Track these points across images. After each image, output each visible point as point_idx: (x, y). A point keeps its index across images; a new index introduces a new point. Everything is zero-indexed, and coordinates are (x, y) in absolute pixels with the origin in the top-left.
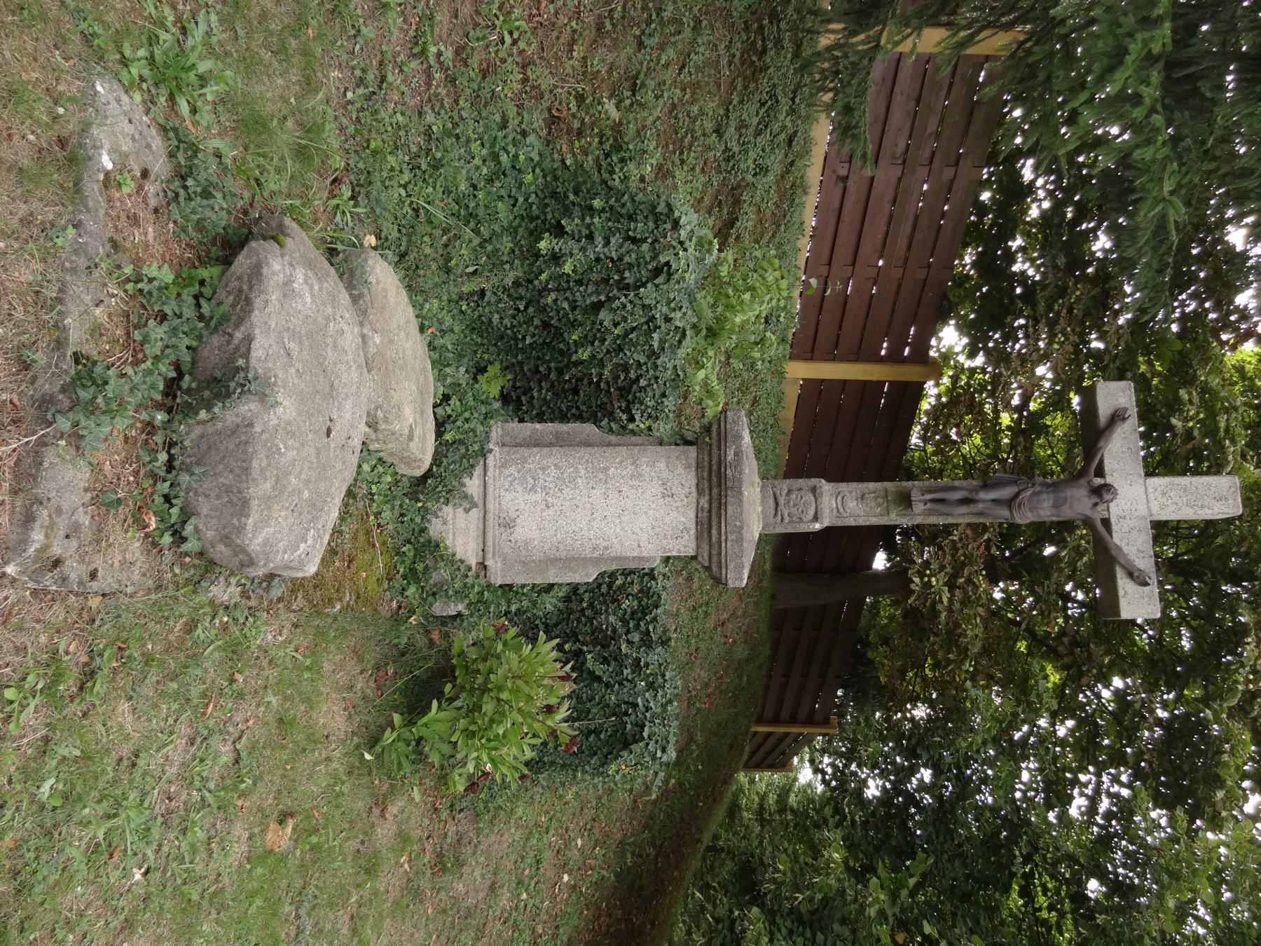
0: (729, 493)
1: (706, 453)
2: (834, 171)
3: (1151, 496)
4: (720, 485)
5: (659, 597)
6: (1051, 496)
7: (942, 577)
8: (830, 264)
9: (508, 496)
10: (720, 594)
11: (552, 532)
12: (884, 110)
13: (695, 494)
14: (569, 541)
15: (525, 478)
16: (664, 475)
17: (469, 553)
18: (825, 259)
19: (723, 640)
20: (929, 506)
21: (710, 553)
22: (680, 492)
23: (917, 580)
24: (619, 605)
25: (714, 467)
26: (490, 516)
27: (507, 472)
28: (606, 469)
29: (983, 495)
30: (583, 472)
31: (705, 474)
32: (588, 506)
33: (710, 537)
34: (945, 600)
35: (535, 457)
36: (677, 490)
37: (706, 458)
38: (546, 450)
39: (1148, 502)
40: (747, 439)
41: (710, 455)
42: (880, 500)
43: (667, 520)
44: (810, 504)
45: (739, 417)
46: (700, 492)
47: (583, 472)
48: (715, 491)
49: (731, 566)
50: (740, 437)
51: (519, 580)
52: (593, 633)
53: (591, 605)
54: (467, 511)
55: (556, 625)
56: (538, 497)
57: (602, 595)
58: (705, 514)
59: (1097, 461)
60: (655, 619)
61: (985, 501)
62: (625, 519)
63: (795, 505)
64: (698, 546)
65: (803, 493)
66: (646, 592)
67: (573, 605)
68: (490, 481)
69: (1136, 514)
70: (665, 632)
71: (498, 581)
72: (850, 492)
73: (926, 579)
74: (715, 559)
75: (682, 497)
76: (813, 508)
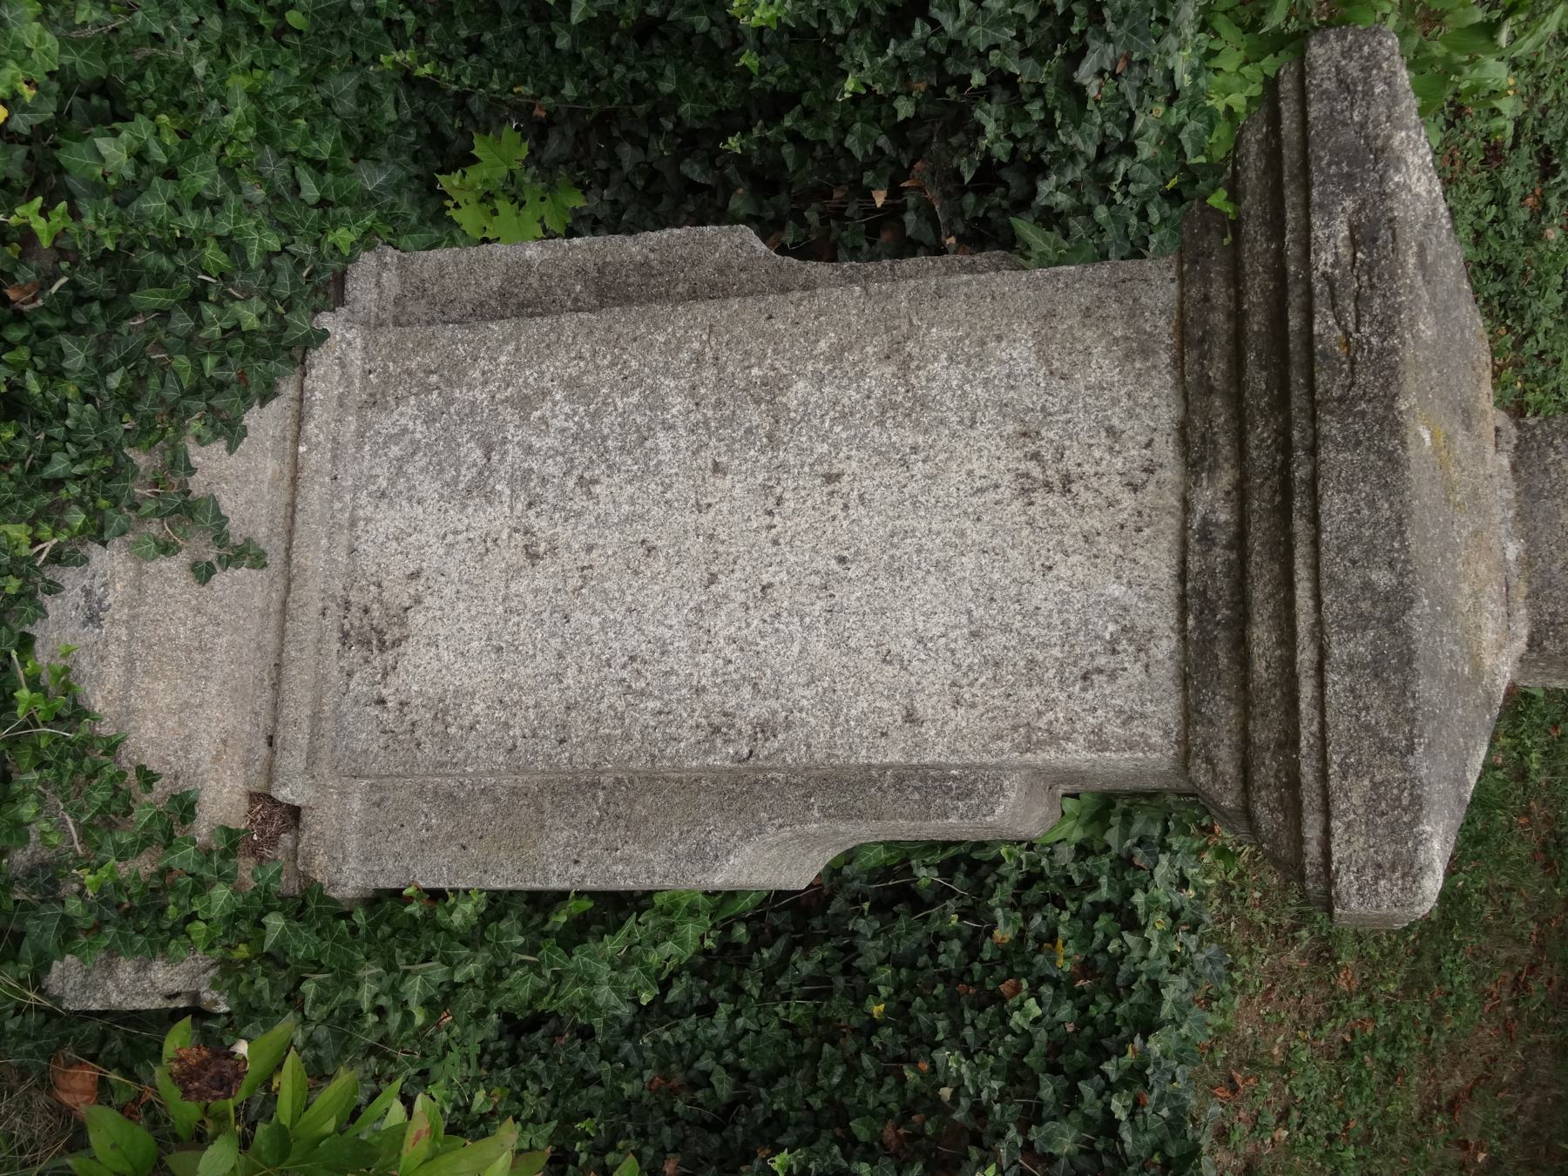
0: (1330, 426)
1: (1217, 272)
4: (1282, 401)
5: (1155, 988)
9: (387, 521)
10: (1438, 1012)
11: (546, 662)
13: (1171, 473)
14: (612, 697)
15: (452, 444)
16: (1028, 396)
17: (204, 750)
21: (1245, 744)
22: (1102, 467)
24: (1004, 1018)
26: (310, 594)
27: (385, 424)
28: (774, 386)
30: (678, 404)
31: (1217, 370)
32: (695, 545)
33: (1243, 661)
35: (498, 357)
36: (1088, 456)
37: (1220, 293)
38: (536, 328)
40: (1416, 179)
41: (1236, 278)
43: (1041, 594)
45: (1371, 64)
46: (1195, 460)
47: (678, 404)
48: (1261, 433)
49: (1352, 797)
50: (1373, 156)
51: (431, 872)
52: (907, 1112)
53: (901, 1013)
54: (203, 573)
55: (770, 1079)
56: (496, 517)
57: (946, 977)
58: (1220, 556)
60: (1136, 1076)
62: (850, 596)
64: (1190, 714)
66: (1102, 972)
67: (837, 1008)
68: (315, 459)
70: (1175, 1125)
71: (349, 878)
74: (1268, 768)
75: (1114, 487)
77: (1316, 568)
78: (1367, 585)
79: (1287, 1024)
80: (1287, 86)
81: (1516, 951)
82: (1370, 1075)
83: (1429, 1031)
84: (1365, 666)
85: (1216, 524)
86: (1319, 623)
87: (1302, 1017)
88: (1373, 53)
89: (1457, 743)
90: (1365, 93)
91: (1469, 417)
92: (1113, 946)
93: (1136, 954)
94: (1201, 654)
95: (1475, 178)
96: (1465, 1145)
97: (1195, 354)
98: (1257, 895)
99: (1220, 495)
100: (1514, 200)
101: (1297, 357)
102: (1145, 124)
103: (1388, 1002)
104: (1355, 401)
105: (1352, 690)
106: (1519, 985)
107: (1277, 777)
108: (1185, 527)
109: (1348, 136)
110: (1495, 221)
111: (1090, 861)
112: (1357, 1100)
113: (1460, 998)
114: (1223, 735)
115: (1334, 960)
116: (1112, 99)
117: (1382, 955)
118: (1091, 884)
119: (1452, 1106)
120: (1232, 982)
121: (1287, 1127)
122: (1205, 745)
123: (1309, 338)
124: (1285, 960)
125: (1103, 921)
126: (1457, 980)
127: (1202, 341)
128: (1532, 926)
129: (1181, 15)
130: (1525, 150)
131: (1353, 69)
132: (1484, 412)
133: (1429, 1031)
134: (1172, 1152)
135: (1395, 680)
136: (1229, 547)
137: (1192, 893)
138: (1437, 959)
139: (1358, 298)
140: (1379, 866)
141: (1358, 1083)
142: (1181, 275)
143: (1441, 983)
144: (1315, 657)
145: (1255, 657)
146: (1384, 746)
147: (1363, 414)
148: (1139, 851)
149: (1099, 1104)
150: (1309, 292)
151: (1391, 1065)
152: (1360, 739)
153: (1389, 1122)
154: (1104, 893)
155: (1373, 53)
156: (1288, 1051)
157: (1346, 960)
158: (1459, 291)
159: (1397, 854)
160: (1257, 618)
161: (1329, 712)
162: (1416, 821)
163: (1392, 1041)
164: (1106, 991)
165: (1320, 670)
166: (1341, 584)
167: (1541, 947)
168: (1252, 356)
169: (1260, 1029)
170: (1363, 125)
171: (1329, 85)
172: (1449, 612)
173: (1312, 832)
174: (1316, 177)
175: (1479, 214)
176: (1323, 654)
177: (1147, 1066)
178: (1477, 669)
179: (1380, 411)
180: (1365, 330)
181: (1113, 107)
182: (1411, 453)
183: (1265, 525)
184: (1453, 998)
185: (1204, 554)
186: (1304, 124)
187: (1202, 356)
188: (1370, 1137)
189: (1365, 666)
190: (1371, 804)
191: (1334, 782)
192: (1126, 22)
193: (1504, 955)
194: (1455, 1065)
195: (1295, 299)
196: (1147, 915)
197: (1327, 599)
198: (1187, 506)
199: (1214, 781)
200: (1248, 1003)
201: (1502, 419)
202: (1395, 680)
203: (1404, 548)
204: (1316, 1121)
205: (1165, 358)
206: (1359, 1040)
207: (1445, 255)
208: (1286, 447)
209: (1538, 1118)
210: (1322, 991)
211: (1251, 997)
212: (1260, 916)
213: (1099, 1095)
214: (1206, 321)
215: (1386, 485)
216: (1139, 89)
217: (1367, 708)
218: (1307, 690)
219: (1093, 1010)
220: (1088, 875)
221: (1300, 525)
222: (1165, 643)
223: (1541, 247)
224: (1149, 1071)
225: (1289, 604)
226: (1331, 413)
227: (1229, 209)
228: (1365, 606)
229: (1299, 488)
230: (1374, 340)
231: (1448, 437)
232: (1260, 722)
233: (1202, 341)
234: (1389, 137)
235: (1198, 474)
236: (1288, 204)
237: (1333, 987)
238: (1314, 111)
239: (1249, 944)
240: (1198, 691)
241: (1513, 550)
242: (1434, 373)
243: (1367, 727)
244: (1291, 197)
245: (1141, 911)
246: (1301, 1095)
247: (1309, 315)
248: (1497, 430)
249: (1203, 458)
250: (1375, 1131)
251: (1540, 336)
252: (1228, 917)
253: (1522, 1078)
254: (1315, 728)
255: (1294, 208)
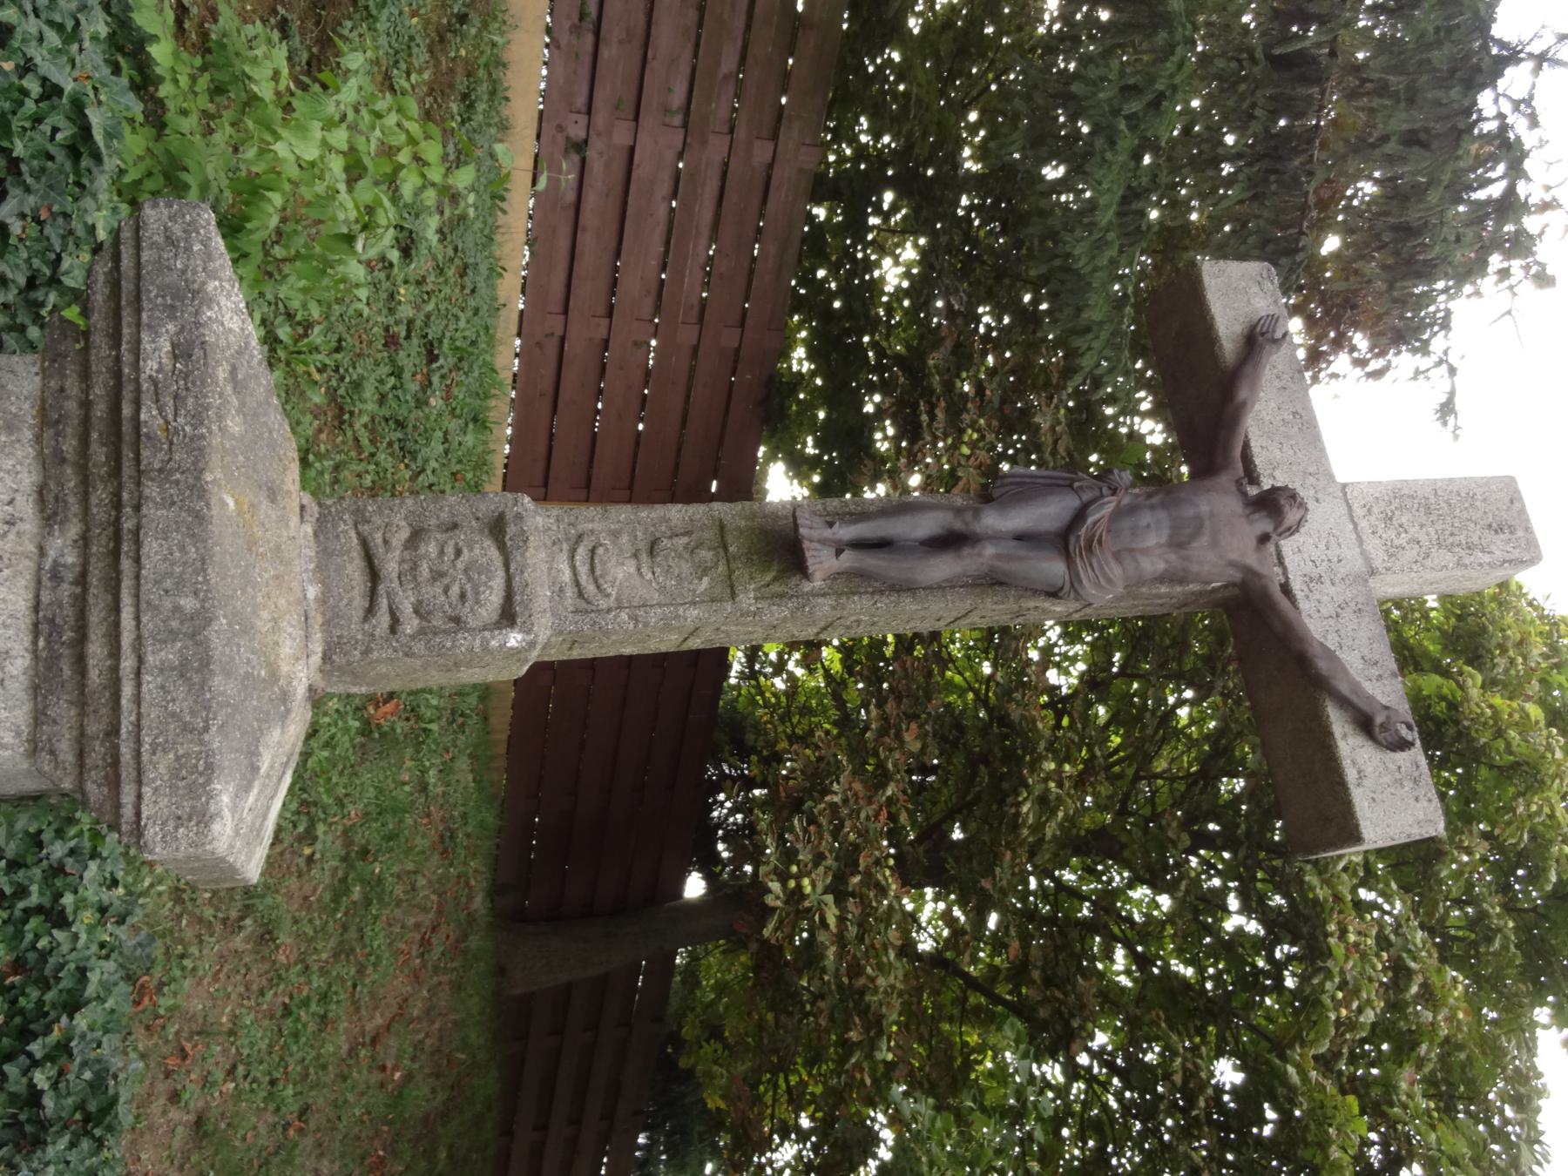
0: (151, 490)
1: (71, 370)
2: (560, 128)
3: (1363, 524)
4: (116, 471)
5: (82, 972)
6: (1162, 515)
7: (822, 876)
8: (566, 312)
10: (361, 971)
12: (641, 20)
18: (555, 303)
19: (376, 1077)
20: (848, 559)
23: (775, 886)
25: (100, 410)
29: (993, 521)
31: (69, 446)
33: (80, 662)
34: (832, 921)
37: (73, 386)
39: (1360, 541)
41: (85, 375)
42: (706, 555)
44: (487, 571)
46: (49, 510)
48: (100, 494)
49: (159, 768)
50: (187, 297)
58: (66, 591)
59: (1238, 452)
61: (996, 537)
63: (437, 575)
64: (39, 717)
65: (461, 537)
69: (1342, 571)
70: (98, 1085)
72: (615, 534)
73: (792, 884)
76: (498, 582)
77: (137, 596)
78: (177, 609)
79: (233, 997)
80: (126, 234)
81: (422, 918)
82: (305, 1026)
83: (355, 986)
84: (174, 669)
85: (64, 566)
86: (139, 638)
87: (247, 989)
88: (193, 221)
89: (250, 725)
90: (186, 249)
91: (274, 493)
92: (43, 943)
93: (65, 948)
94: (49, 669)
95: (379, 356)
96: (383, 1068)
97: (52, 432)
98: (207, 895)
99: (69, 542)
100: (407, 375)
101: (128, 437)
102: (71, 266)
103: (321, 968)
104: (171, 472)
105: (163, 687)
106: (425, 943)
107: (104, 759)
108: (40, 569)
109: (172, 278)
110: (394, 388)
111: (21, 873)
112: (295, 1048)
113: (379, 958)
114: (65, 731)
115: (274, 940)
116: (37, 240)
117: (315, 931)
118: (22, 892)
119: (374, 1041)
120: (183, 968)
121: (234, 1080)
122: (50, 740)
123: (137, 423)
124: (231, 945)
125: (34, 923)
126: (375, 944)
127: (58, 422)
128: (434, 897)
129: (96, 184)
130: (415, 341)
131: (177, 230)
132: (289, 492)
133: (355, 986)
134: (92, 1107)
135: (196, 678)
136: (75, 583)
137: (121, 891)
138: (360, 930)
139: (176, 397)
140: (179, 818)
141: (296, 1035)
142: (43, 370)
143: (364, 947)
144: (135, 665)
145: (90, 667)
146: (186, 728)
147: (177, 482)
148: (70, 860)
149: (24, 1080)
150: (138, 390)
151: (324, 1017)
152: (167, 724)
153: (322, 1061)
154: (34, 899)
155: (193, 221)
156: (235, 1018)
157: (283, 938)
158: (269, 404)
159: (193, 807)
160: (93, 637)
161: (144, 705)
162: (209, 781)
163: (324, 998)
164: (36, 983)
165: (138, 673)
166: (156, 608)
167: (440, 912)
168: (95, 435)
169: (209, 1004)
170: (184, 272)
171: (159, 239)
172: (247, 629)
173: (127, 798)
174: (145, 304)
175: (381, 382)
176: (141, 660)
177: (71, 1040)
178: (274, 675)
179: (191, 481)
180: (181, 420)
181: (38, 247)
182: (214, 512)
183: (101, 565)
184: (373, 958)
185: (54, 588)
186: (138, 265)
187: (57, 434)
188: (307, 1075)
189: (174, 669)
190: (175, 773)
191: (145, 757)
192: (43, 179)
193: (411, 921)
194: (376, 1008)
195: (127, 394)
196: (75, 912)
197: (144, 619)
198: (42, 552)
199: (56, 768)
200: (199, 984)
201: (307, 499)
202: (196, 678)
203: (206, 581)
204: (258, 1072)
205: (28, 435)
206: (296, 1001)
207: (256, 377)
208: (117, 505)
209: (440, 1039)
210: (266, 966)
211: (201, 979)
212: (208, 912)
213: (25, 1072)
214: (61, 408)
215: (194, 535)
216: (63, 237)
217: (174, 700)
218: (127, 690)
219: (22, 1001)
220: (19, 885)
221: (126, 564)
222: (19, 662)
223: (427, 410)
224: (73, 1044)
225: (117, 624)
226: (153, 480)
227: (81, 322)
228: (174, 624)
229: (126, 536)
230: (188, 429)
231: (252, 505)
232: (92, 717)
233: (58, 422)
234: (204, 283)
235: (51, 526)
236: (124, 323)
237: (274, 962)
238: (145, 256)
239: (199, 936)
240: (45, 697)
241: (312, 592)
242: (241, 458)
243: (173, 714)
244: (127, 317)
245: (69, 910)
246: (245, 1052)
247: (137, 405)
248: (302, 507)
249: (55, 514)
250: (312, 1070)
251: (429, 472)
252: (180, 917)
253: (428, 1012)
254: (133, 718)
255: (129, 325)
